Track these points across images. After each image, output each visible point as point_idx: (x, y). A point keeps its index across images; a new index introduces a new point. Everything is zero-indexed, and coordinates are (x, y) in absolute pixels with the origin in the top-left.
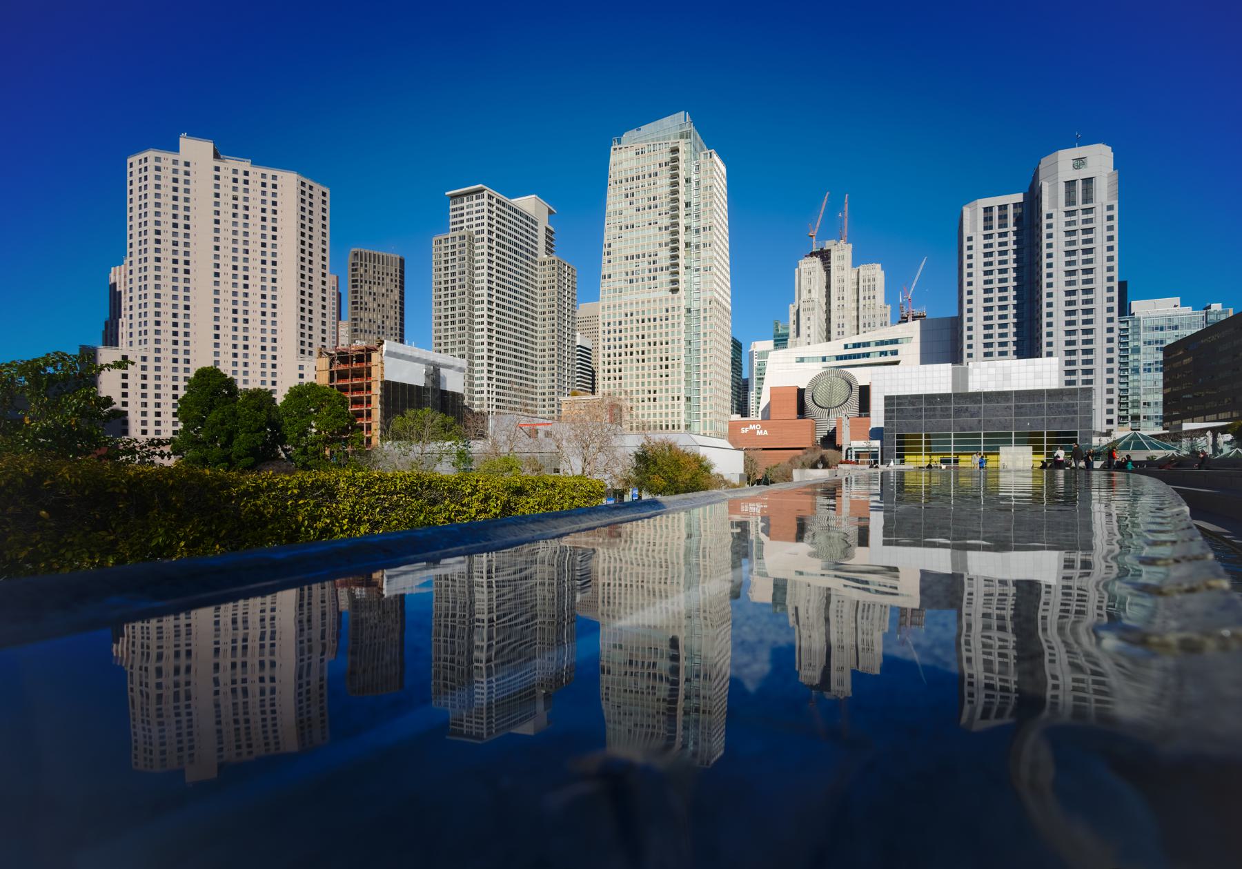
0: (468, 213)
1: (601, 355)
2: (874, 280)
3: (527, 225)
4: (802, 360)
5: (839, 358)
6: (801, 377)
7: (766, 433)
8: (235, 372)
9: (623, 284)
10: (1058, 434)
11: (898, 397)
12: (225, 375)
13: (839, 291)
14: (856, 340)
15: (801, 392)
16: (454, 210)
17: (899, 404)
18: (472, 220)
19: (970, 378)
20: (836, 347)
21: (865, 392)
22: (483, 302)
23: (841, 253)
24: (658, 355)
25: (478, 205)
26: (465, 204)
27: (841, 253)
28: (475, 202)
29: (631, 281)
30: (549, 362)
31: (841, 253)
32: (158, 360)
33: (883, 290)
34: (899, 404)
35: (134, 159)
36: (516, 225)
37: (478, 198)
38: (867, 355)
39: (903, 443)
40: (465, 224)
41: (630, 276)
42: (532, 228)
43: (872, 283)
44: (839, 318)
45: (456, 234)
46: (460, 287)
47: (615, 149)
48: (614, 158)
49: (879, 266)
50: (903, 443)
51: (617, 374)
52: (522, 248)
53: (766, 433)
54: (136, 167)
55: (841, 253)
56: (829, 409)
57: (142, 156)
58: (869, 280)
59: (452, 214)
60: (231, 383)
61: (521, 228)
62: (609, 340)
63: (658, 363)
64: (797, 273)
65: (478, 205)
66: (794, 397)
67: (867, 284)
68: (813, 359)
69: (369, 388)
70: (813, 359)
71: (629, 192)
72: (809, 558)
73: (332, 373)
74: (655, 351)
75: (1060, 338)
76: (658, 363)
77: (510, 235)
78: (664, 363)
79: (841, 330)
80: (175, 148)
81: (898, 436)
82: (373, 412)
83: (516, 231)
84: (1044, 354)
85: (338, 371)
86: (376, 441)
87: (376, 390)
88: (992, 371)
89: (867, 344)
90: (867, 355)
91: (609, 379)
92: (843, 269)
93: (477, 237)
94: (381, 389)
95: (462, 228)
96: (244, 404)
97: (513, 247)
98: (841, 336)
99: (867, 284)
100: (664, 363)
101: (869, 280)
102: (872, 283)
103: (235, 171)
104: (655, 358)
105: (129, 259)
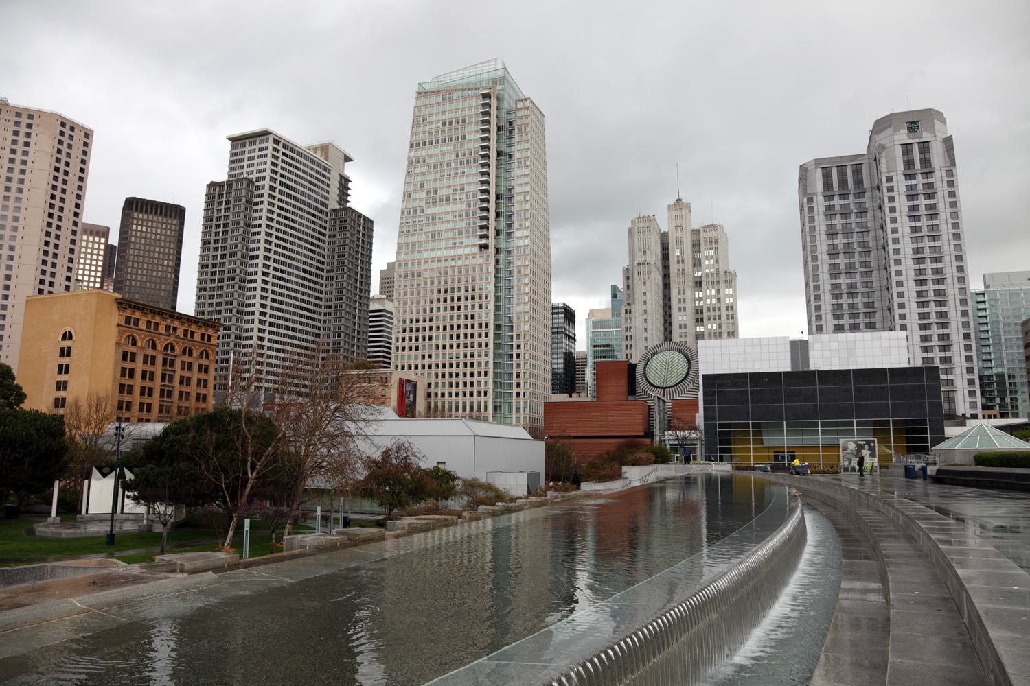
2: (716, 242)
3: (318, 172)
10: (906, 423)
11: (720, 376)
17: (720, 385)
18: (253, 158)
19: (811, 353)
21: (570, 315)
22: (253, 321)
25: (261, 149)
26: (247, 148)
28: (258, 146)
34: (720, 385)
36: (304, 179)
37: (262, 142)
39: (729, 434)
40: (245, 170)
44: (679, 283)
46: (229, 271)
50: (729, 434)
51: (413, 344)
58: (711, 242)
61: (311, 175)
65: (261, 149)
75: (913, 310)
79: (682, 305)
81: (721, 426)
83: (301, 210)
84: (898, 327)
88: (835, 346)
91: (404, 349)
93: (257, 184)
97: (309, 329)
101: (711, 242)
104: (480, 356)
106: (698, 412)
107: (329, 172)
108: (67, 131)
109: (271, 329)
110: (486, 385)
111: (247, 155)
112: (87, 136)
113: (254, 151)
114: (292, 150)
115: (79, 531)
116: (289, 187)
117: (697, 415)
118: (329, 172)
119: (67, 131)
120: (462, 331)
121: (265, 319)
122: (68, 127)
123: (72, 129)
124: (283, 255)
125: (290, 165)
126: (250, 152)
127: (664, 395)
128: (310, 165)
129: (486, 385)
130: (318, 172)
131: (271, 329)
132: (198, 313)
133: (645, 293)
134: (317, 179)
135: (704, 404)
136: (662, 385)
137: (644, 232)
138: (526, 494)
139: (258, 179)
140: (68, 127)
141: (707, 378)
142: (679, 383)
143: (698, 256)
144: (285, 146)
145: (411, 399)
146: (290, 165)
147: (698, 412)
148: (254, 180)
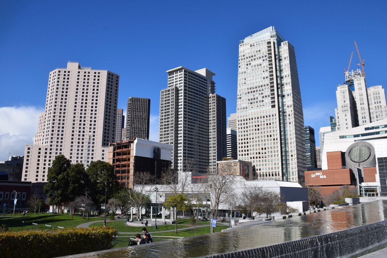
0: (176, 79)
1: (237, 128)
2: (379, 93)
3: (197, 79)
4: (342, 137)
5: (363, 135)
6: (343, 146)
7: (325, 177)
8: (71, 157)
9: (247, 105)
12: (66, 159)
13: (361, 100)
14: (370, 125)
15: (343, 154)
16: (170, 78)
18: (177, 81)
20: (360, 130)
23: (359, 83)
24: (254, 124)
25: (180, 75)
26: (175, 75)
27: (359, 82)
28: (179, 74)
29: (251, 103)
30: (213, 144)
31: (359, 82)
32: (51, 149)
33: (384, 98)
35: (52, 73)
38: (378, 133)
41: (251, 101)
42: (205, 83)
43: (378, 95)
44: (362, 114)
45: (170, 88)
47: (241, 45)
48: (241, 49)
49: (381, 86)
52: (200, 92)
53: (325, 177)
54: (52, 75)
55: (359, 83)
56: (359, 162)
57: (54, 71)
58: (376, 94)
59: (168, 80)
60: (68, 162)
62: (241, 125)
63: (254, 128)
64: (213, 106)
66: (340, 157)
67: (375, 96)
68: (350, 136)
69: (129, 160)
70: (350, 136)
71: (248, 63)
72: (215, 73)
73: (114, 154)
74: (252, 122)
76: (254, 128)
77: (200, 89)
78: (257, 128)
80: (65, 67)
82: (130, 170)
85: (117, 152)
86: (131, 186)
87: (132, 161)
89: (378, 128)
90: (378, 133)
92: (361, 90)
94: (134, 160)
95: (172, 86)
96: (73, 171)
98: (364, 123)
99: (375, 96)
100: (257, 128)
101: (376, 94)
102: (378, 95)
103: (85, 73)
105: (46, 110)
106: (376, 173)
107: (207, 81)
108: (111, 76)
109: (189, 146)
110: (278, 165)
111: (175, 78)
112: (117, 77)
113: (177, 76)
114: (192, 74)
115: (181, 217)
116: (192, 89)
117: (376, 175)
118: (207, 81)
119: (111, 76)
120: (260, 139)
121: (186, 142)
122: (111, 75)
123: (112, 75)
124: (191, 116)
125: (191, 82)
126: (176, 76)
127: (359, 166)
128: (196, 77)
129: (278, 165)
130: (197, 79)
131: (189, 146)
132: (160, 141)
133: (346, 120)
134: (197, 82)
135: (379, 170)
136: (358, 161)
137: (344, 93)
138: (350, 183)
139: (180, 87)
140: (111, 75)
141: (378, 159)
142: (366, 160)
143: (360, 135)
144: (189, 73)
145: (247, 172)
146: (191, 82)
147: (376, 173)
148: (178, 87)
